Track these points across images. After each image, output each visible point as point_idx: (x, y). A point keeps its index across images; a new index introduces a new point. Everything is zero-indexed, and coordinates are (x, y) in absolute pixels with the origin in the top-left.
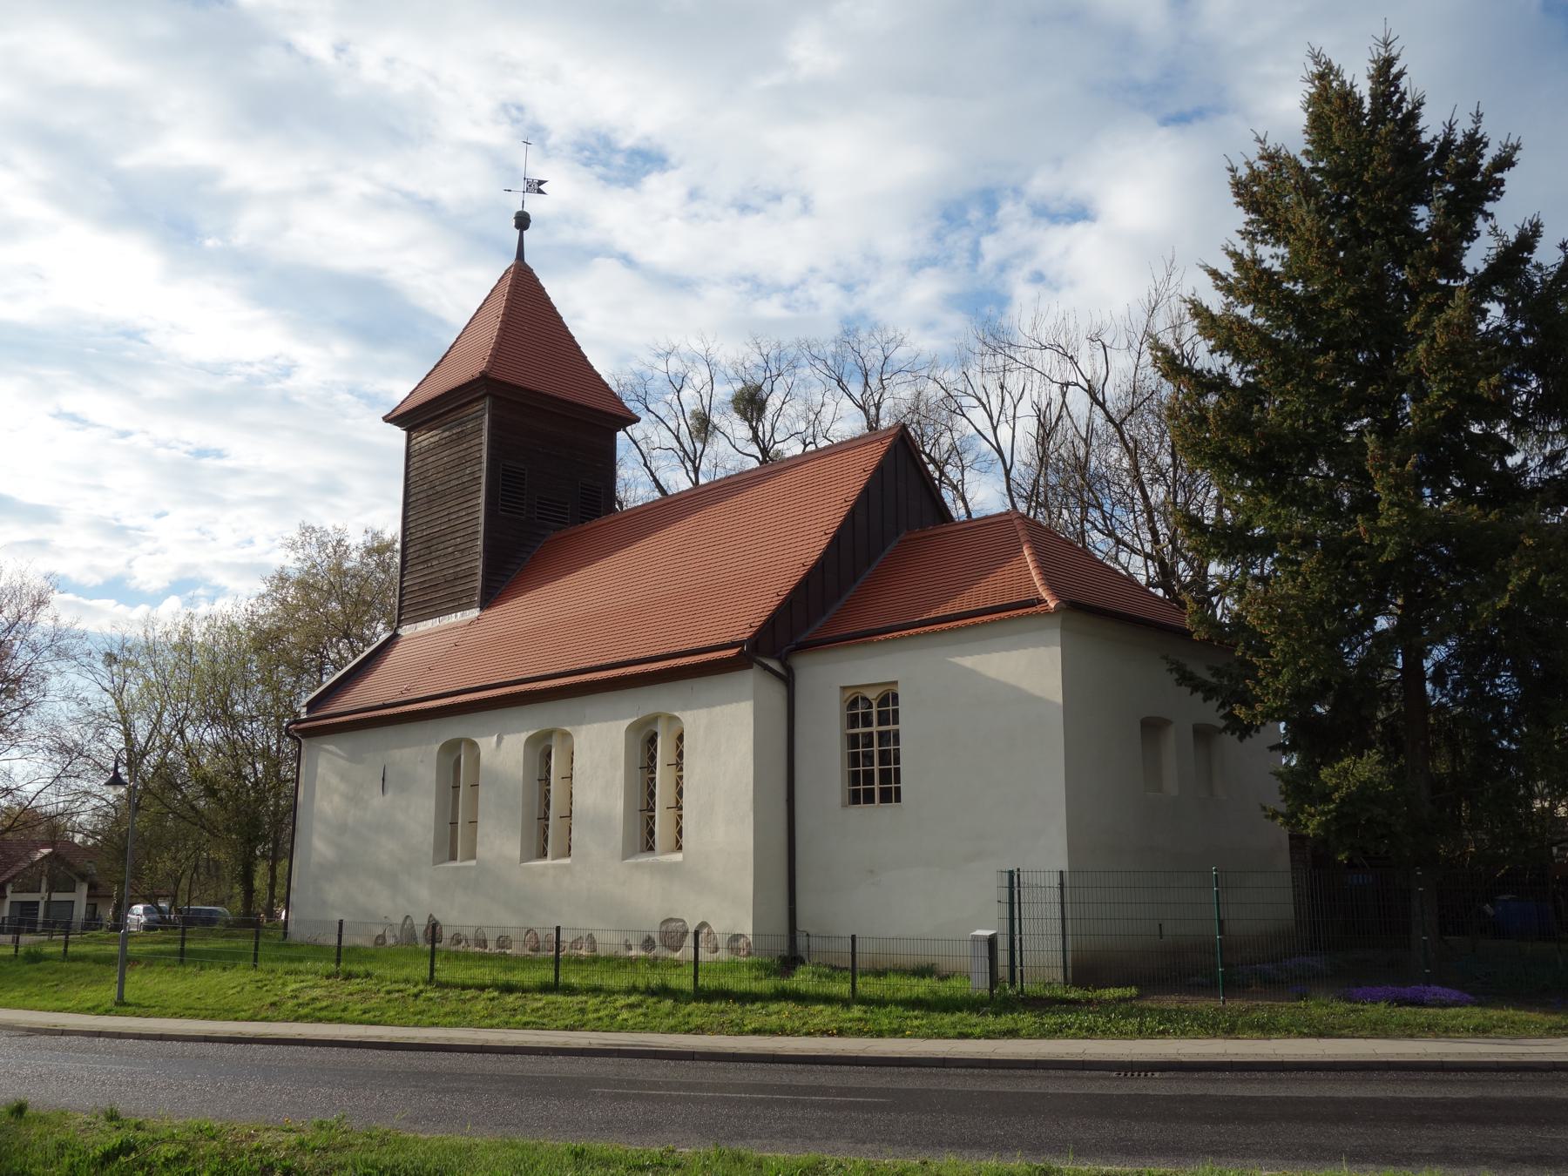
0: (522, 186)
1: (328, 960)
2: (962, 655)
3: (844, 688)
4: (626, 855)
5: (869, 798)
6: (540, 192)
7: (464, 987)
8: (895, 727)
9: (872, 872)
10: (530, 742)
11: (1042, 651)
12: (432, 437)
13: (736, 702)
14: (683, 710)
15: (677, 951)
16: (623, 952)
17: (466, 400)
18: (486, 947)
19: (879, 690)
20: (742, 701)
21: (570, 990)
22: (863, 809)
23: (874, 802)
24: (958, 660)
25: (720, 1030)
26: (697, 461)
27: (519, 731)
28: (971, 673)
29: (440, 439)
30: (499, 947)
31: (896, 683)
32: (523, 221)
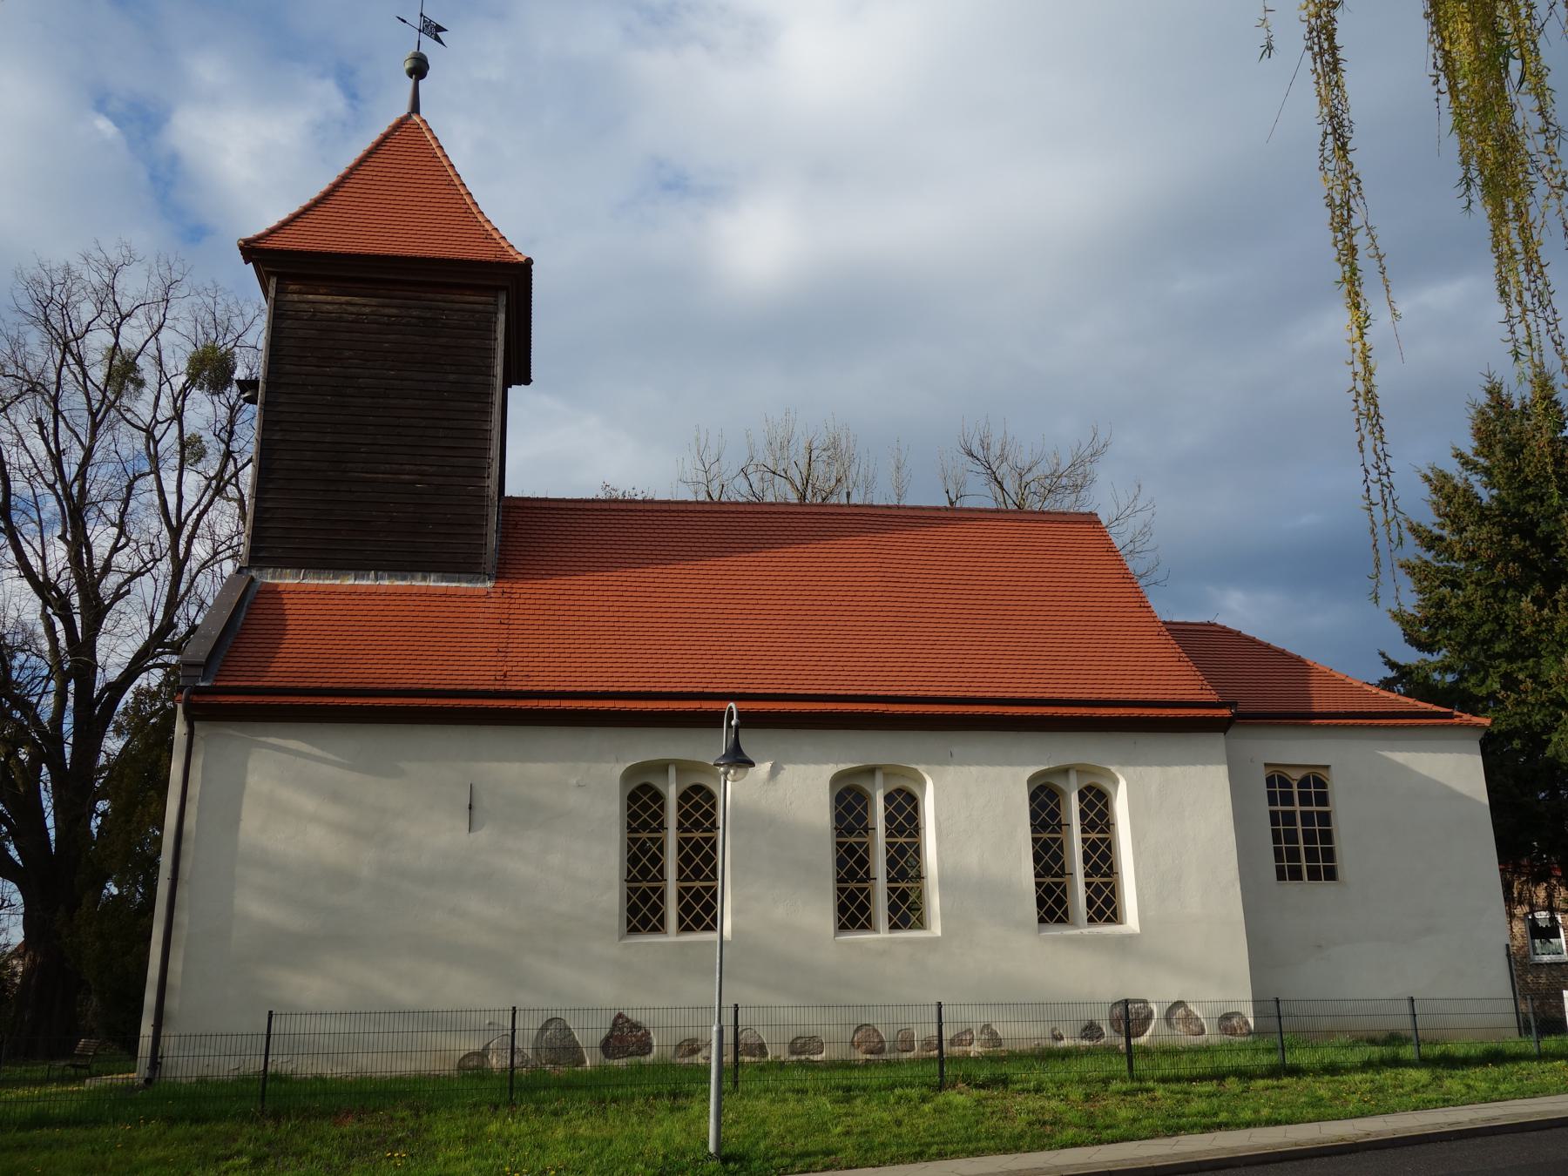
0: (416, 21)
1: (1139, 1047)
2: (267, 736)
3: (1266, 765)
4: (621, 938)
5: (1296, 875)
6: (438, 39)
7: (1219, 1076)
8: (1275, 808)
9: (1320, 946)
10: (837, 779)
11: (1465, 757)
12: (365, 305)
13: (1202, 764)
14: (1122, 764)
15: (821, 1052)
16: (1049, 1043)
17: (392, 277)
18: (765, 1054)
19: (1303, 773)
20: (1211, 764)
21: (1295, 1071)
22: (1290, 886)
23: (1301, 878)
24: (1400, 757)
25: (1521, 1094)
26: (99, 417)
27: (827, 762)
28: (1403, 769)
29: (372, 314)
30: (793, 1053)
31: (1327, 767)
32: (419, 69)
